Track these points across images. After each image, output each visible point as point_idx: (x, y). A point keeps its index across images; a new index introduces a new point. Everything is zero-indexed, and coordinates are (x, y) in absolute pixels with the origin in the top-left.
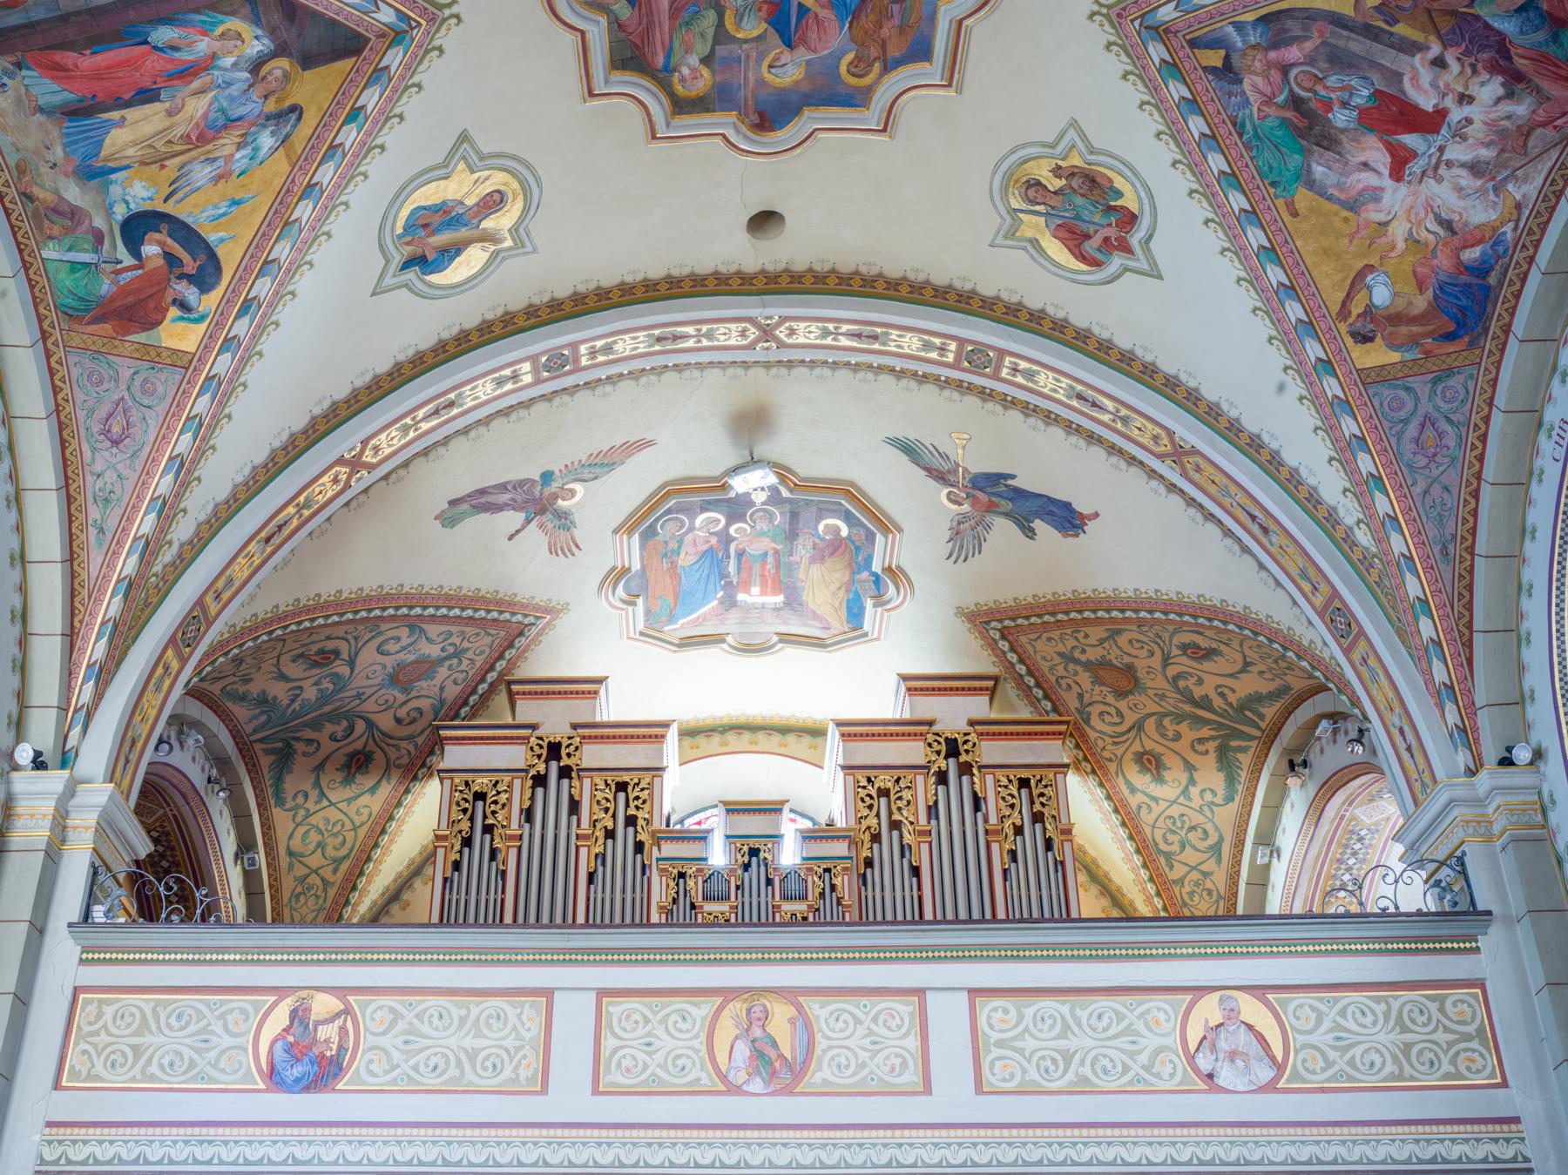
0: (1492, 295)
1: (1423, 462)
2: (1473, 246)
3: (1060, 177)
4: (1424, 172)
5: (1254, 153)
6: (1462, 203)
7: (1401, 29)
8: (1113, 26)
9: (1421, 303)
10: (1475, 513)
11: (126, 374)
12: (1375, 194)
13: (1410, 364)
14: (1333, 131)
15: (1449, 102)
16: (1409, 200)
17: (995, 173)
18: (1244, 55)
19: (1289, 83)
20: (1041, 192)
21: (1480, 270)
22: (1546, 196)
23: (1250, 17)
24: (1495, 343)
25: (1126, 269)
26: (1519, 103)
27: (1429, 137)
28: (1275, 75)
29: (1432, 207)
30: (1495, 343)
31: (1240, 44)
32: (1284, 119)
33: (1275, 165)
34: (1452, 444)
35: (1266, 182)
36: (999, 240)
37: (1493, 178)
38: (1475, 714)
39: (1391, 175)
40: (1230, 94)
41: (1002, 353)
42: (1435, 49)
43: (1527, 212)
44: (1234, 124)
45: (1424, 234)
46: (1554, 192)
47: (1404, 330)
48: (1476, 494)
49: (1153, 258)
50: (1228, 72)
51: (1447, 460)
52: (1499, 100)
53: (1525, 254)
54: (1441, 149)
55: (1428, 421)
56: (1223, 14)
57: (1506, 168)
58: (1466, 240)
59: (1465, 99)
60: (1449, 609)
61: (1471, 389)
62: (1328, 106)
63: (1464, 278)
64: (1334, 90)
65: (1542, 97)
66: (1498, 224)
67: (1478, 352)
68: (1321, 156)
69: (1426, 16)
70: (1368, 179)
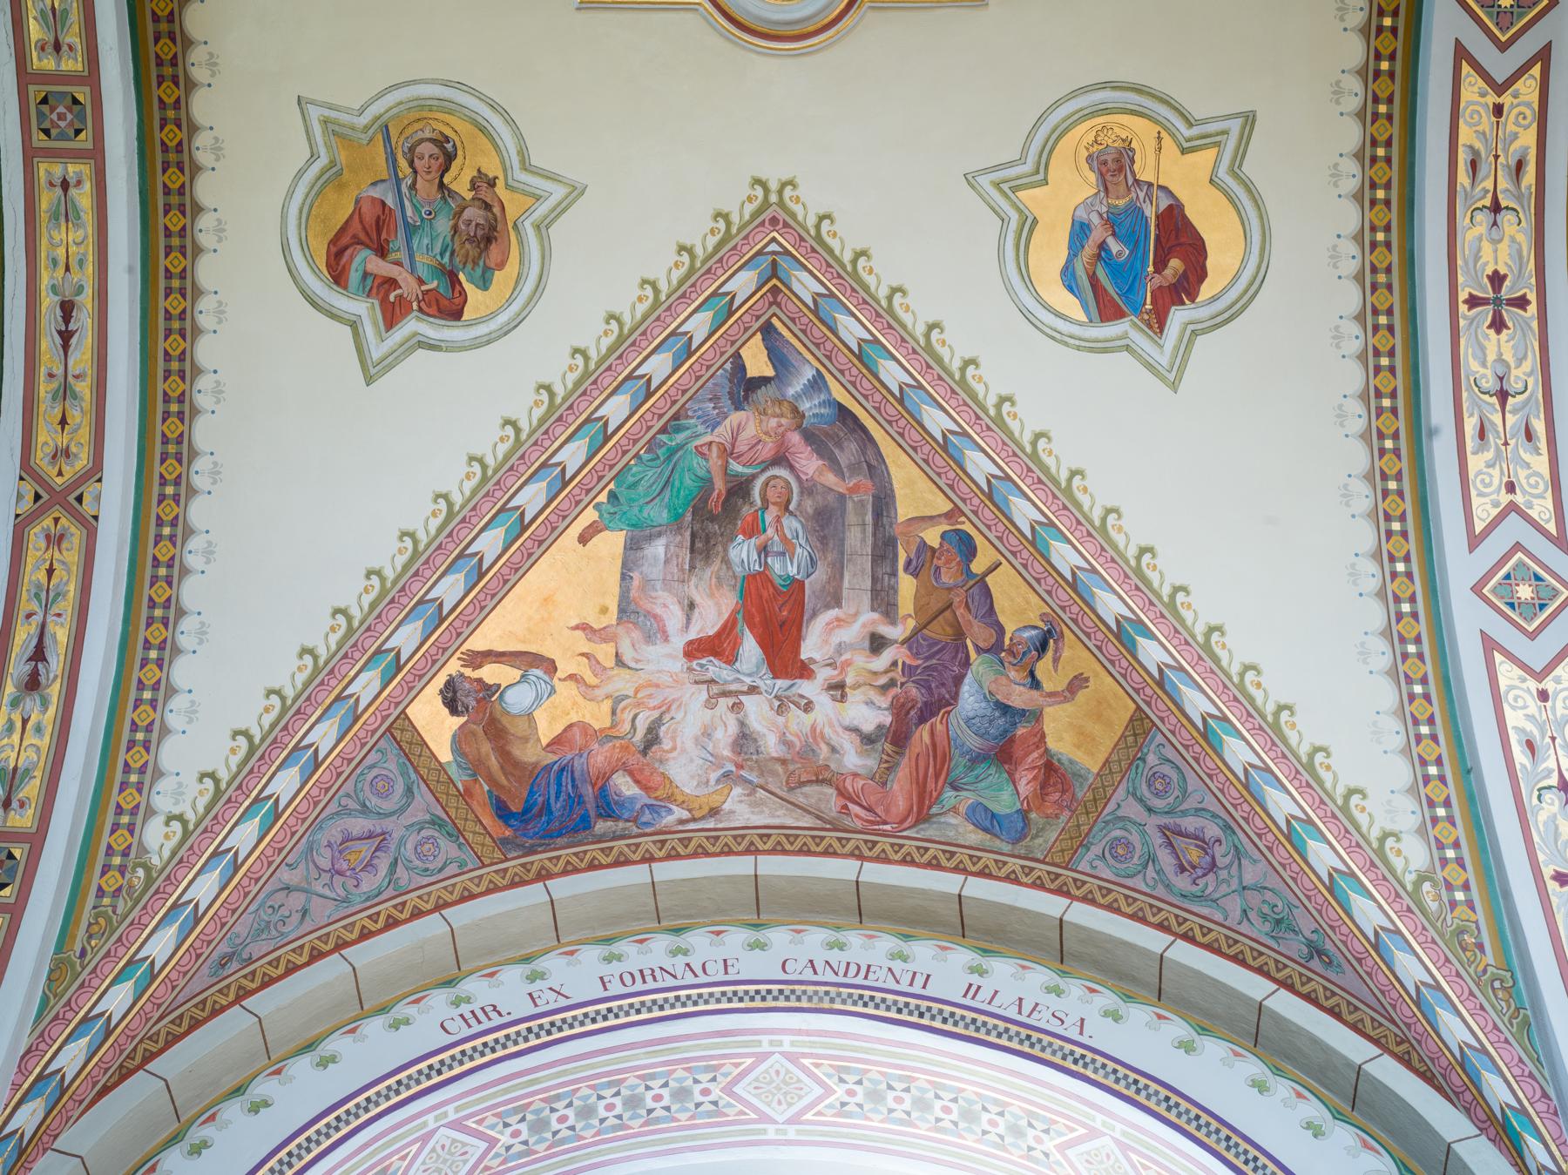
0: (580, 837)
1: (325, 863)
2: (637, 782)
3: (474, 186)
4: (712, 681)
5: (646, 457)
6: (690, 745)
7: (907, 586)
8: (754, 215)
9: (530, 754)
10: (292, 969)
11: (1133, 810)
12: (656, 632)
13: (443, 778)
14: (720, 548)
15: (823, 675)
16: (666, 679)
17: (446, 84)
18: (779, 402)
19: (763, 471)
20: (435, 164)
21: (608, 807)
22: (743, 837)
23: (839, 394)
24: (519, 870)
25: (354, 325)
26: (860, 754)
27: (765, 669)
28: (767, 451)
29: (668, 709)
30: (519, 870)
31: (791, 392)
32: (710, 481)
33: (641, 489)
34: (365, 887)
35: (612, 486)
36: (315, 113)
37: (740, 767)
38: (45, 1150)
39: (690, 643)
40: (715, 399)
41: (97, 155)
42: (896, 632)
43: (711, 825)
44: (676, 417)
45: (628, 716)
46: (752, 843)
47: (486, 747)
48: (316, 956)
49: (398, 361)
50: (745, 388)
51: (342, 893)
52: (856, 730)
53: (653, 849)
54: (753, 690)
55: (380, 840)
56: (829, 358)
57: (762, 774)
58: (641, 770)
59: (838, 689)
60: (157, 1015)
61: (448, 872)
62: (753, 530)
63: (588, 792)
64: (779, 529)
65: (881, 779)
66: (680, 799)
67: (498, 855)
68: (680, 546)
69: (940, 605)
70: (673, 616)
